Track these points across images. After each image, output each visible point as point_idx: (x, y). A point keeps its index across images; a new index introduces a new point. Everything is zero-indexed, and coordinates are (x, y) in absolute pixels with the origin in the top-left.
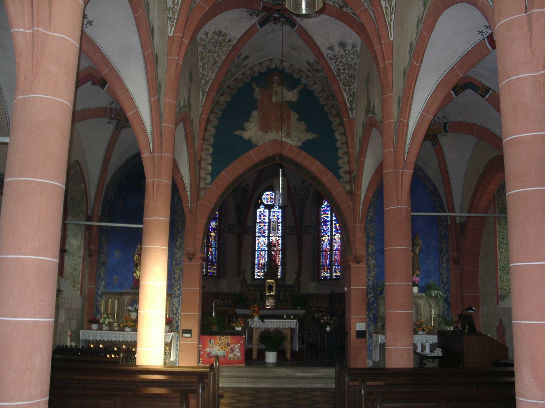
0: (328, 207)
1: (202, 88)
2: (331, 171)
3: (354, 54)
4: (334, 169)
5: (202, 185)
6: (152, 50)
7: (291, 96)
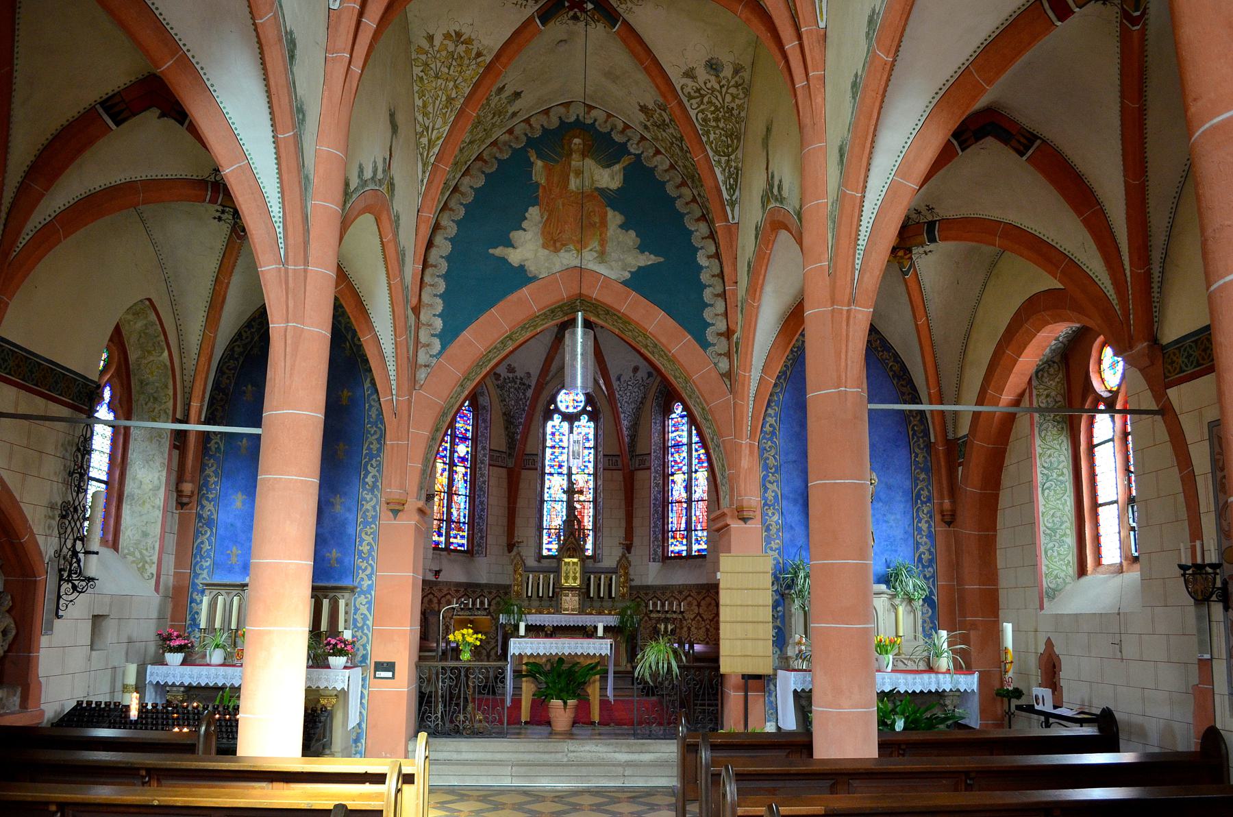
0: (682, 417)
1: (422, 155)
2: (689, 333)
3: (737, 86)
4: (697, 329)
5: (422, 358)
6: (275, 17)
7: (608, 178)
